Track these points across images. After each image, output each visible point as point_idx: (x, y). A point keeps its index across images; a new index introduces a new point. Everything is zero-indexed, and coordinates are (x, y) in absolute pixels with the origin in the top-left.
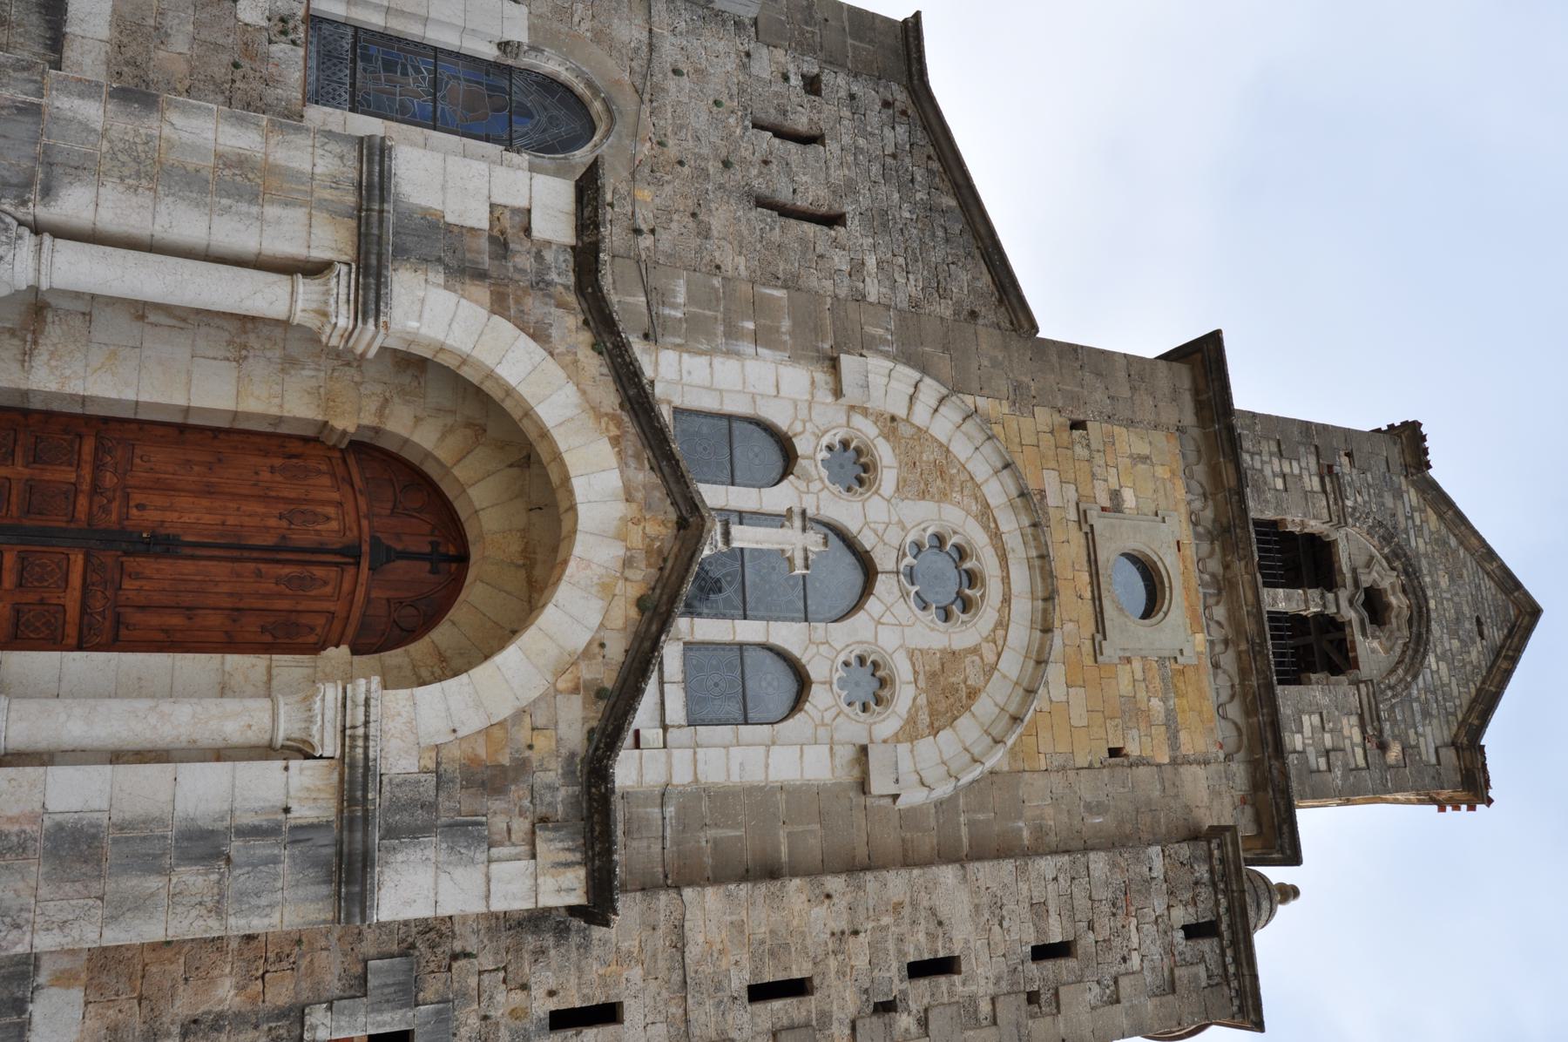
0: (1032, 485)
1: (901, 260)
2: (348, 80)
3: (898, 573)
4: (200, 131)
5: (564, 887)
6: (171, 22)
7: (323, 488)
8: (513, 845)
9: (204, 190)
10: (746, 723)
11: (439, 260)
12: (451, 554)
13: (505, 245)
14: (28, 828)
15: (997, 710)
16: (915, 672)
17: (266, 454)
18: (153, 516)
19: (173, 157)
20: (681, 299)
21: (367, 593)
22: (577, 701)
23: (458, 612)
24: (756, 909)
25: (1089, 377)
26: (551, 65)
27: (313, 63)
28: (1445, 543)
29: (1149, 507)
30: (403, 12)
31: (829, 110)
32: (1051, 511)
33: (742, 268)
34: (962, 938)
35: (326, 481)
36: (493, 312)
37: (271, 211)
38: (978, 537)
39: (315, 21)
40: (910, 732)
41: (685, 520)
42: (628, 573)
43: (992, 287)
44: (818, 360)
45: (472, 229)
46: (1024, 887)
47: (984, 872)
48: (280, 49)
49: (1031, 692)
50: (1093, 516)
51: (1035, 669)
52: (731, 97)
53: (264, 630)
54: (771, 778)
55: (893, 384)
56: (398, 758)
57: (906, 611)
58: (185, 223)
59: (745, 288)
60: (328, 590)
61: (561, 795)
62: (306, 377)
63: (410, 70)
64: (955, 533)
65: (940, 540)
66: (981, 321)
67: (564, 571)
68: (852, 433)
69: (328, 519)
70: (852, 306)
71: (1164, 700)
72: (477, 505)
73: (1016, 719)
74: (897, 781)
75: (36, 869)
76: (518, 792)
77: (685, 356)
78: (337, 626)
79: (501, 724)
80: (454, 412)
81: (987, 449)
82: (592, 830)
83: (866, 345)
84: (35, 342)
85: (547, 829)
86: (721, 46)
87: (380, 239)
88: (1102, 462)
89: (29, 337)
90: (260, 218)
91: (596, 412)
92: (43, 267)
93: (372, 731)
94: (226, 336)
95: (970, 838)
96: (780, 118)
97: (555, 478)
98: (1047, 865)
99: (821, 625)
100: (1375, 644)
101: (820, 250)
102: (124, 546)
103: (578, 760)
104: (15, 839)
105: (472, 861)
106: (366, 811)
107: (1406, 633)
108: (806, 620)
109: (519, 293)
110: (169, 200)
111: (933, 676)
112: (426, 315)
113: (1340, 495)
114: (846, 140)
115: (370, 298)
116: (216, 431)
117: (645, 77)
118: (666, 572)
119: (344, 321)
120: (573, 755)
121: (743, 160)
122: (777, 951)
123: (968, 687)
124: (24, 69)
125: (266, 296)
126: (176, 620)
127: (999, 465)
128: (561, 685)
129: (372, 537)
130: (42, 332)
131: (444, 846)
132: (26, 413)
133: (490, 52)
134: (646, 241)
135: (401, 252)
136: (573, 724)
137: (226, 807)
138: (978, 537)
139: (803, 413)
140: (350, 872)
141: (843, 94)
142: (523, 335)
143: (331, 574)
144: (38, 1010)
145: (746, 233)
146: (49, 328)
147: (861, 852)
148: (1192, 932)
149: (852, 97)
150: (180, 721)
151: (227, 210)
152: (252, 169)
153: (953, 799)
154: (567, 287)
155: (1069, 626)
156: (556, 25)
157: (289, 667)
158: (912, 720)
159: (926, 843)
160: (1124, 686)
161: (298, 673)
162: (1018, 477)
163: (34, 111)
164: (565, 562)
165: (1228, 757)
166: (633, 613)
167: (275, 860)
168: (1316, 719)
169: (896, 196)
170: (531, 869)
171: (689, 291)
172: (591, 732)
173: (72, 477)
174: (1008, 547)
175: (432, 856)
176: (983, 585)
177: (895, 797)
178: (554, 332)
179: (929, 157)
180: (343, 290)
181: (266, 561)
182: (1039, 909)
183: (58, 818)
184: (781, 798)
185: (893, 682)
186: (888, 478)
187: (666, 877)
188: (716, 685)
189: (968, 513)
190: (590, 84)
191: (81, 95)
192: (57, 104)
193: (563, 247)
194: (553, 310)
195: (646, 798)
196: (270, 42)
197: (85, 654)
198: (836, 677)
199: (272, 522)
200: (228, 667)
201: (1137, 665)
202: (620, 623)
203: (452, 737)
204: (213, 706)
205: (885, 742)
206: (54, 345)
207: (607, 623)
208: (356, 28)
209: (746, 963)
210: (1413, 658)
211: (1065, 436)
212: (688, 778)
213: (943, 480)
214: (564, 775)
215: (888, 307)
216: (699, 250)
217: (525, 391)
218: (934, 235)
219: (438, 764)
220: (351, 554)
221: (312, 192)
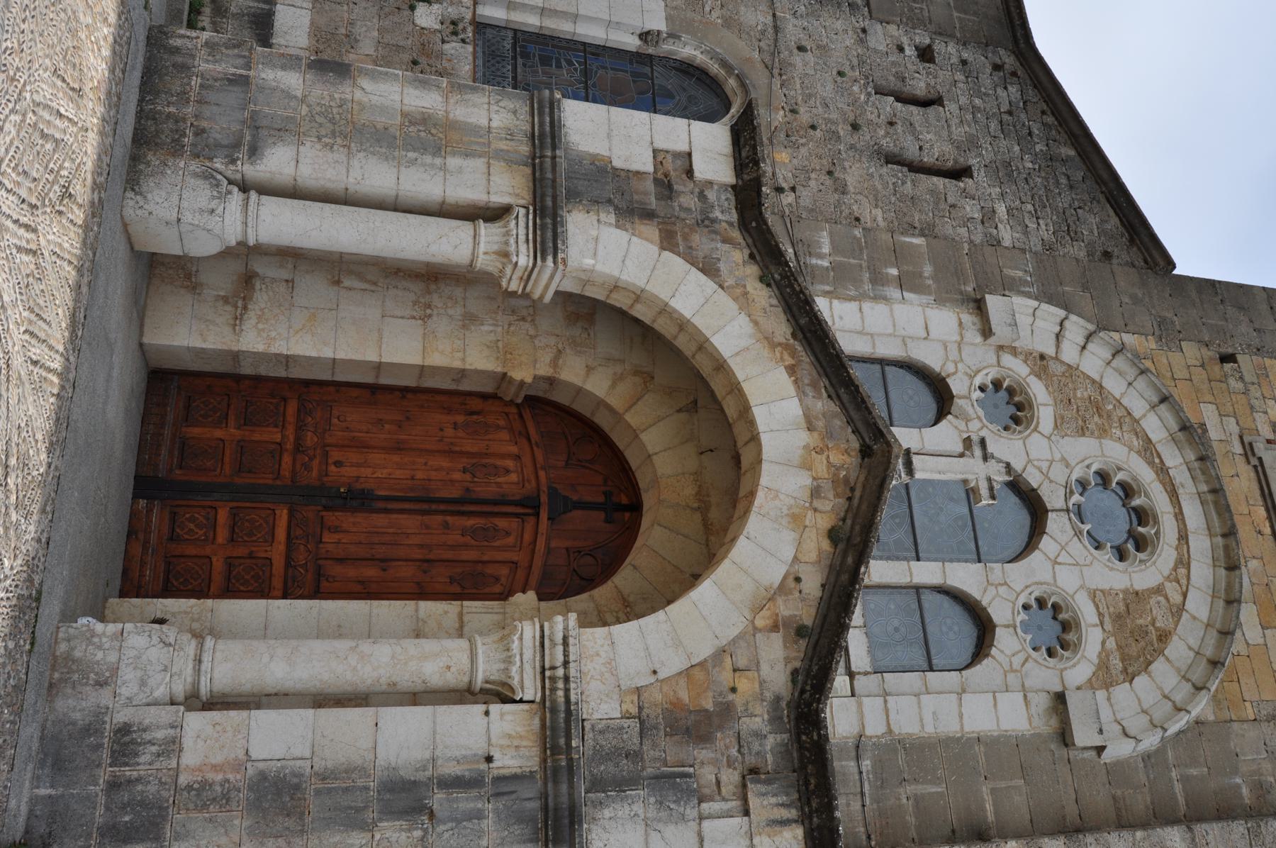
1: (1030, 207)
2: (510, 75)
3: (1068, 510)
4: (388, 94)
6: (359, 30)
7: (503, 443)
8: (724, 799)
9: (392, 145)
10: (931, 670)
11: (609, 201)
12: (623, 505)
13: (670, 186)
14: (231, 777)
15: (1192, 654)
16: (1100, 615)
17: (449, 411)
18: (349, 471)
19: (364, 118)
20: (826, 249)
21: (548, 540)
22: (777, 640)
23: (639, 555)
25: (1231, 311)
26: (687, 50)
27: (480, 62)
30: (556, 11)
31: (944, 75)
32: (1215, 444)
33: (880, 219)
35: (504, 435)
36: (663, 248)
37: (453, 162)
38: (1145, 475)
39: (481, 27)
40: (1103, 679)
41: (869, 447)
42: (816, 504)
43: (1121, 229)
44: (963, 302)
45: (638, 173)
48: (452, 47)
49: (1226, 634)
50: (1260, 448)
51: (1226, 609)
52: (852, 68)
53: (452, 580)
54: (967, 729)
55: (1039, 323)
56: (600, 704)
57: (1080, 549)
58: (375, 175)
59: (886, 237)
60: (510, 540)
62: (485, 332)
63: (564, 63)
64: (1120, 469)
65: (1104, 478)
66: (1115, 261)
67: (751, 503)
68: (1004, 372)
69: (508, 471)
70: (988, 250)
72: (651, 450)
73: (1215, 664)
74: (1101, 732)
75: (239, 822)
76: (724, 739)
77: (835, 302)
78: (521, 574)
79: (702, 664)
80: (622, 361)
81: (1141, 383)
82: (807, 783)
83: (1007, 287)
84: (245, 308)
85: (759, 781)
86: (839, 25)
88: (1258, 394)
89: (240, 304)
90: (443, 168)
92: (250, 219)
93: (572, 672)
94: (412, 297)
96: (899, 84)
97: (731, 411)
99: (997, 566)
101: (951, 200)
102: (324, 501)
103: (784, 704)
104: (218, 789)
105: (683, 818)
106: (570, 760)
108: (979, 561)
109: (686, 230)
110: (362, 154)
112: (601, 252)
114: (963, 100)
115: (548, 238)
116: (405, 390)
117: (773, 54)
118: (856, 502)
119: (524, 260)
120: (778, 699)
121: (870, 122)
123: (1157, 629)
124: (235, 46)
125: (449, 243)
126: (371, 572)
127: (1155, 399)
128: (760, 623)
129: (549, 488)
130: (251, 299)
131: (652, 800)
132: (238, 378)
133: (631, 42)
134: (788, 198)
135: (574, 196)
136: (775, 664)
137: (427, 755)
138: (1145, 475)
139: (954, 354)
140: (557, 829)
141: (954, 60)
142: (694, 269)
143: (514, 524)
145: (880, 187)
146: (257, 295)
147: (1072, 810)
149: (964, 62)
152: (435, 125)
153: (1160, 751)
154: (731, 224)
155: (1253, 564)
156: (690, 14)
159: (1140, 801)
161: (488, 619)
162: (1177, 410)
163: (243, 81)
164: (752, 494)
166: (826, 545)
167: (479, 815)
169: (1017, 148)
170: (746, 828)
171: (832, 242)
172: (795, 673)
173: (278, 437)
174: (1177, 481)
175: (641, 812)
176: (1156, 522)
177: (1100, 750)
178: (722, 265)
179: (1043, 113)
180: (522, 231)
181: (453, 513)
183: (261, 765)
184: (979, 750)
185: (1078, 625)
186: (1045, 416)
187: (869, 837)
188: (896, 630)
189: (1131, 449)
190: (724, 64)
191: (284, 68)
192: (263, 75)
193: (724, 187)
194: (719, 245)
196: (443, 42)
197: (289, 601)
198: (1018, 619)
199: (457, 476)
200: (422, 614)
202: (813, 556)
203: (652, 679)
204: (412, 647)
205: (1078, 688)
206: (262, 310)
207: (800, 556)
208: (515, 31)
211: (1216, 369)
212: (881, 729)
213: (1100, 416)
214: (772, 721)
215: (1023, 251)
216: (838, 205)
218: (1057, 183)
219: (640, 708)
220: (530, 505)
221: (489, 143)
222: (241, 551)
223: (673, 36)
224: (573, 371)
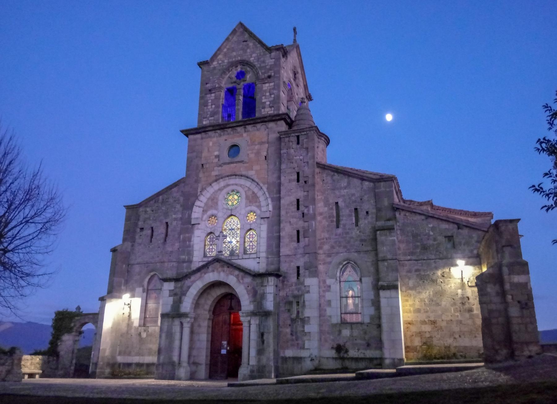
0: (215, 178)
7: (221, 318)
24: (285, 241)
34: (293, 199)
40: (259, 207)
47: (283, 193)
56: (251, 308)
58: (177, 343)
61: (258, 280)
71: (256, 145)
98: (283, 178)
113: (215, 88)
115: (185, 315)
116: (212, 336)
119: (189, 319)
122: (291, 237)
125: (186, 331)
136: (248, 279)
160: (252, 156)
165: (268, 128)
168: (263, 97)
182: (290, 181)
186: (214, 212)
195: (268, 261)
209: (293, 243)
217: (198, 290)
223: (143, 286)
224: (207, 307)
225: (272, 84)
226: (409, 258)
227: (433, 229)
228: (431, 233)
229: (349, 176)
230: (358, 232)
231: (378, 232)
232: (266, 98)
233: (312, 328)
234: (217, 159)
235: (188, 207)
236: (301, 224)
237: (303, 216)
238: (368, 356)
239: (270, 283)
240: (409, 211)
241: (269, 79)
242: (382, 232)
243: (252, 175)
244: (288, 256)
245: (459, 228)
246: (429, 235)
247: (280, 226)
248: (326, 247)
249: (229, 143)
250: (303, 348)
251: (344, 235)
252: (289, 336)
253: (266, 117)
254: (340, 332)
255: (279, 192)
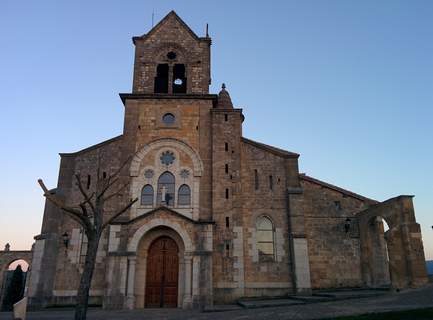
0: (151, 139)
1: (111, 161)
5: (210, 227)
22: (187, 225)
24: (216, 196)
28: (158, 34)
29: (154, 114)
37: (121, 268)
38: (161, 151)
40: (192, 167)
46: (217, 152)
47: (214, 159)
50: (157, 127)
61: (199, 227)
71: (189, 116)
76: (198, 233)
87: (123, 252)
90: (122, 269)
91: (146, 222)
95: (209, 159)
98: (214, 147)
100: (179, 58)
107: (177, 50)
111: (184, 162)
113: (149, 62)
115: (132, 254)
136: (190, 226)
138: (161, 151)
143: (167, 255)
144: (219, 287)
148: (226, 120)
150: (188, 275)
151: (121, 273)
153: (203, 161)
157: (181, 261)
158: (190, 167)
159: (209, 166)
160: (186, 124)
162: (150, 143)
165: (199, 104)
168: (193, 78)
182: (220, 149)
184: (201, 191)
186: (151, 168)
193: (121, 227)
201: (183, 121)
204: (187, 271)
210: (182, 50)
211: (142, 131)
218: (105, 154)
222: (170, 293)
225: (201, 69)
226: (310, 215)
227: (326, 196)
228: (325, 199)
229: (266, 151)
230: (272, 194)
231: (290, 195)
232: (195, 79)
233: (239, 265)
234: (154, 123)
235: (127, 161)
236: (229, 184)
237: (231, 178)
238: (281, 287)
239: (210, 230)
240: (310, 181)
241: (198, 64)
242: (293, 195)
243: (185, 141)
244: (219, 209)
245: (344, 196)
246: (324, 200)
247: (212, 184)
248: (248, 203)
249: (165, 112)
250: (232, 281)
251: (262, 196)
252: (221, 272)
253: (199, 95)
254: (259, 269)
255: (211, 157)
